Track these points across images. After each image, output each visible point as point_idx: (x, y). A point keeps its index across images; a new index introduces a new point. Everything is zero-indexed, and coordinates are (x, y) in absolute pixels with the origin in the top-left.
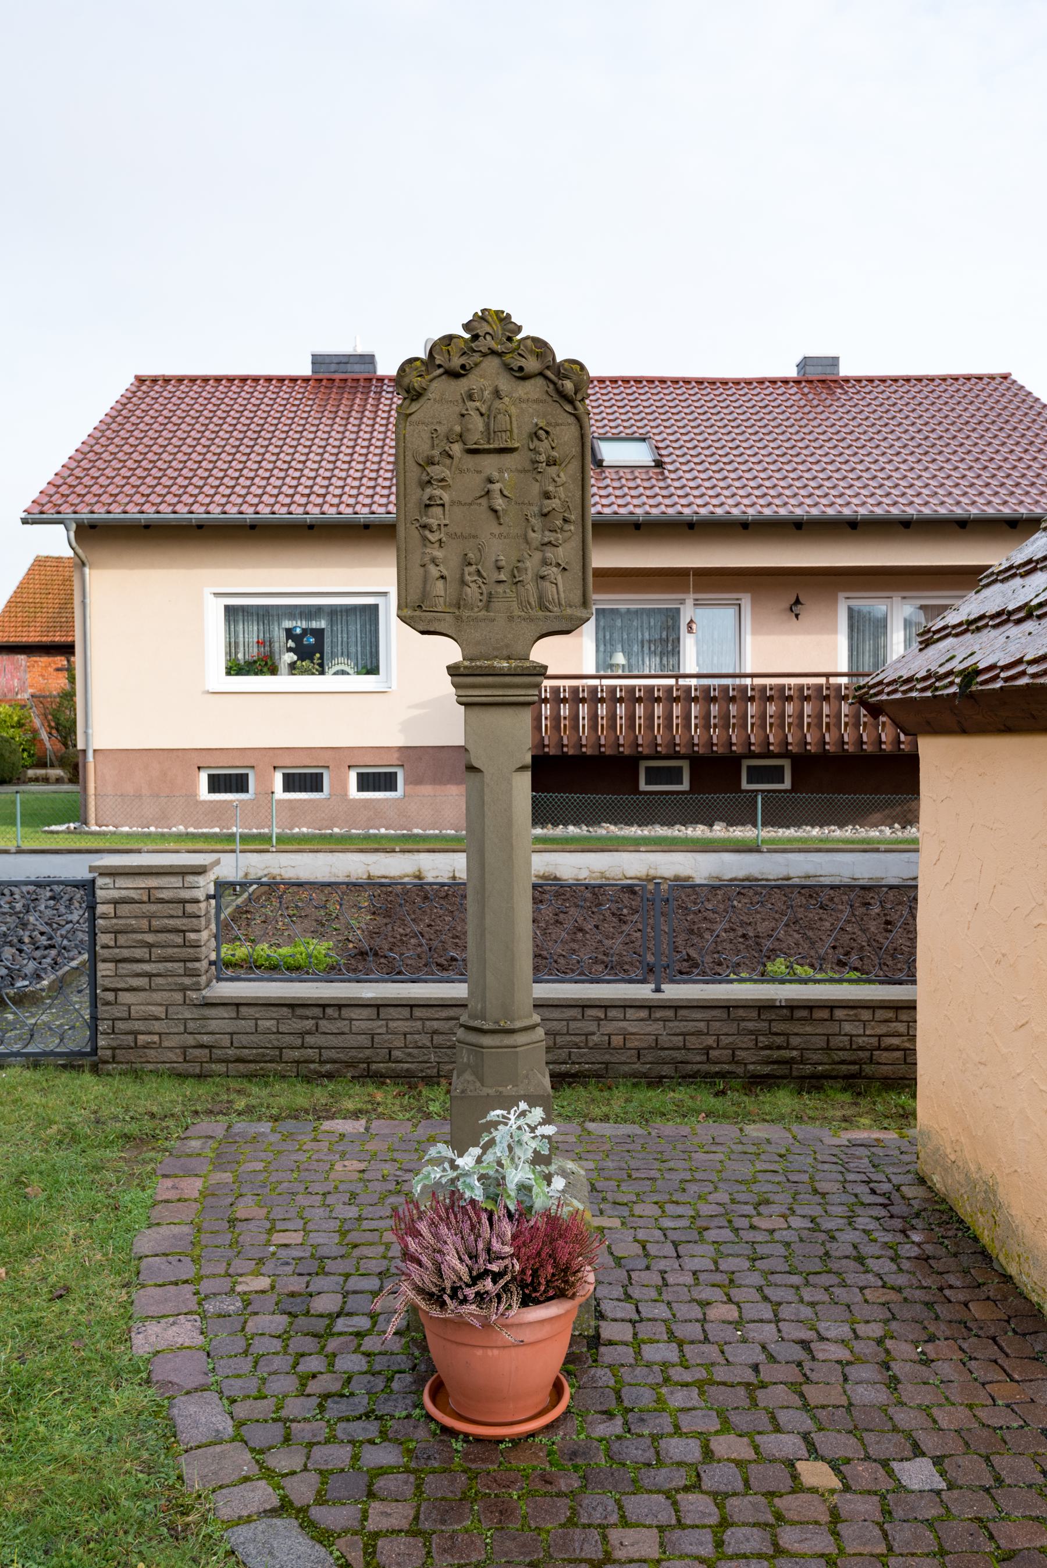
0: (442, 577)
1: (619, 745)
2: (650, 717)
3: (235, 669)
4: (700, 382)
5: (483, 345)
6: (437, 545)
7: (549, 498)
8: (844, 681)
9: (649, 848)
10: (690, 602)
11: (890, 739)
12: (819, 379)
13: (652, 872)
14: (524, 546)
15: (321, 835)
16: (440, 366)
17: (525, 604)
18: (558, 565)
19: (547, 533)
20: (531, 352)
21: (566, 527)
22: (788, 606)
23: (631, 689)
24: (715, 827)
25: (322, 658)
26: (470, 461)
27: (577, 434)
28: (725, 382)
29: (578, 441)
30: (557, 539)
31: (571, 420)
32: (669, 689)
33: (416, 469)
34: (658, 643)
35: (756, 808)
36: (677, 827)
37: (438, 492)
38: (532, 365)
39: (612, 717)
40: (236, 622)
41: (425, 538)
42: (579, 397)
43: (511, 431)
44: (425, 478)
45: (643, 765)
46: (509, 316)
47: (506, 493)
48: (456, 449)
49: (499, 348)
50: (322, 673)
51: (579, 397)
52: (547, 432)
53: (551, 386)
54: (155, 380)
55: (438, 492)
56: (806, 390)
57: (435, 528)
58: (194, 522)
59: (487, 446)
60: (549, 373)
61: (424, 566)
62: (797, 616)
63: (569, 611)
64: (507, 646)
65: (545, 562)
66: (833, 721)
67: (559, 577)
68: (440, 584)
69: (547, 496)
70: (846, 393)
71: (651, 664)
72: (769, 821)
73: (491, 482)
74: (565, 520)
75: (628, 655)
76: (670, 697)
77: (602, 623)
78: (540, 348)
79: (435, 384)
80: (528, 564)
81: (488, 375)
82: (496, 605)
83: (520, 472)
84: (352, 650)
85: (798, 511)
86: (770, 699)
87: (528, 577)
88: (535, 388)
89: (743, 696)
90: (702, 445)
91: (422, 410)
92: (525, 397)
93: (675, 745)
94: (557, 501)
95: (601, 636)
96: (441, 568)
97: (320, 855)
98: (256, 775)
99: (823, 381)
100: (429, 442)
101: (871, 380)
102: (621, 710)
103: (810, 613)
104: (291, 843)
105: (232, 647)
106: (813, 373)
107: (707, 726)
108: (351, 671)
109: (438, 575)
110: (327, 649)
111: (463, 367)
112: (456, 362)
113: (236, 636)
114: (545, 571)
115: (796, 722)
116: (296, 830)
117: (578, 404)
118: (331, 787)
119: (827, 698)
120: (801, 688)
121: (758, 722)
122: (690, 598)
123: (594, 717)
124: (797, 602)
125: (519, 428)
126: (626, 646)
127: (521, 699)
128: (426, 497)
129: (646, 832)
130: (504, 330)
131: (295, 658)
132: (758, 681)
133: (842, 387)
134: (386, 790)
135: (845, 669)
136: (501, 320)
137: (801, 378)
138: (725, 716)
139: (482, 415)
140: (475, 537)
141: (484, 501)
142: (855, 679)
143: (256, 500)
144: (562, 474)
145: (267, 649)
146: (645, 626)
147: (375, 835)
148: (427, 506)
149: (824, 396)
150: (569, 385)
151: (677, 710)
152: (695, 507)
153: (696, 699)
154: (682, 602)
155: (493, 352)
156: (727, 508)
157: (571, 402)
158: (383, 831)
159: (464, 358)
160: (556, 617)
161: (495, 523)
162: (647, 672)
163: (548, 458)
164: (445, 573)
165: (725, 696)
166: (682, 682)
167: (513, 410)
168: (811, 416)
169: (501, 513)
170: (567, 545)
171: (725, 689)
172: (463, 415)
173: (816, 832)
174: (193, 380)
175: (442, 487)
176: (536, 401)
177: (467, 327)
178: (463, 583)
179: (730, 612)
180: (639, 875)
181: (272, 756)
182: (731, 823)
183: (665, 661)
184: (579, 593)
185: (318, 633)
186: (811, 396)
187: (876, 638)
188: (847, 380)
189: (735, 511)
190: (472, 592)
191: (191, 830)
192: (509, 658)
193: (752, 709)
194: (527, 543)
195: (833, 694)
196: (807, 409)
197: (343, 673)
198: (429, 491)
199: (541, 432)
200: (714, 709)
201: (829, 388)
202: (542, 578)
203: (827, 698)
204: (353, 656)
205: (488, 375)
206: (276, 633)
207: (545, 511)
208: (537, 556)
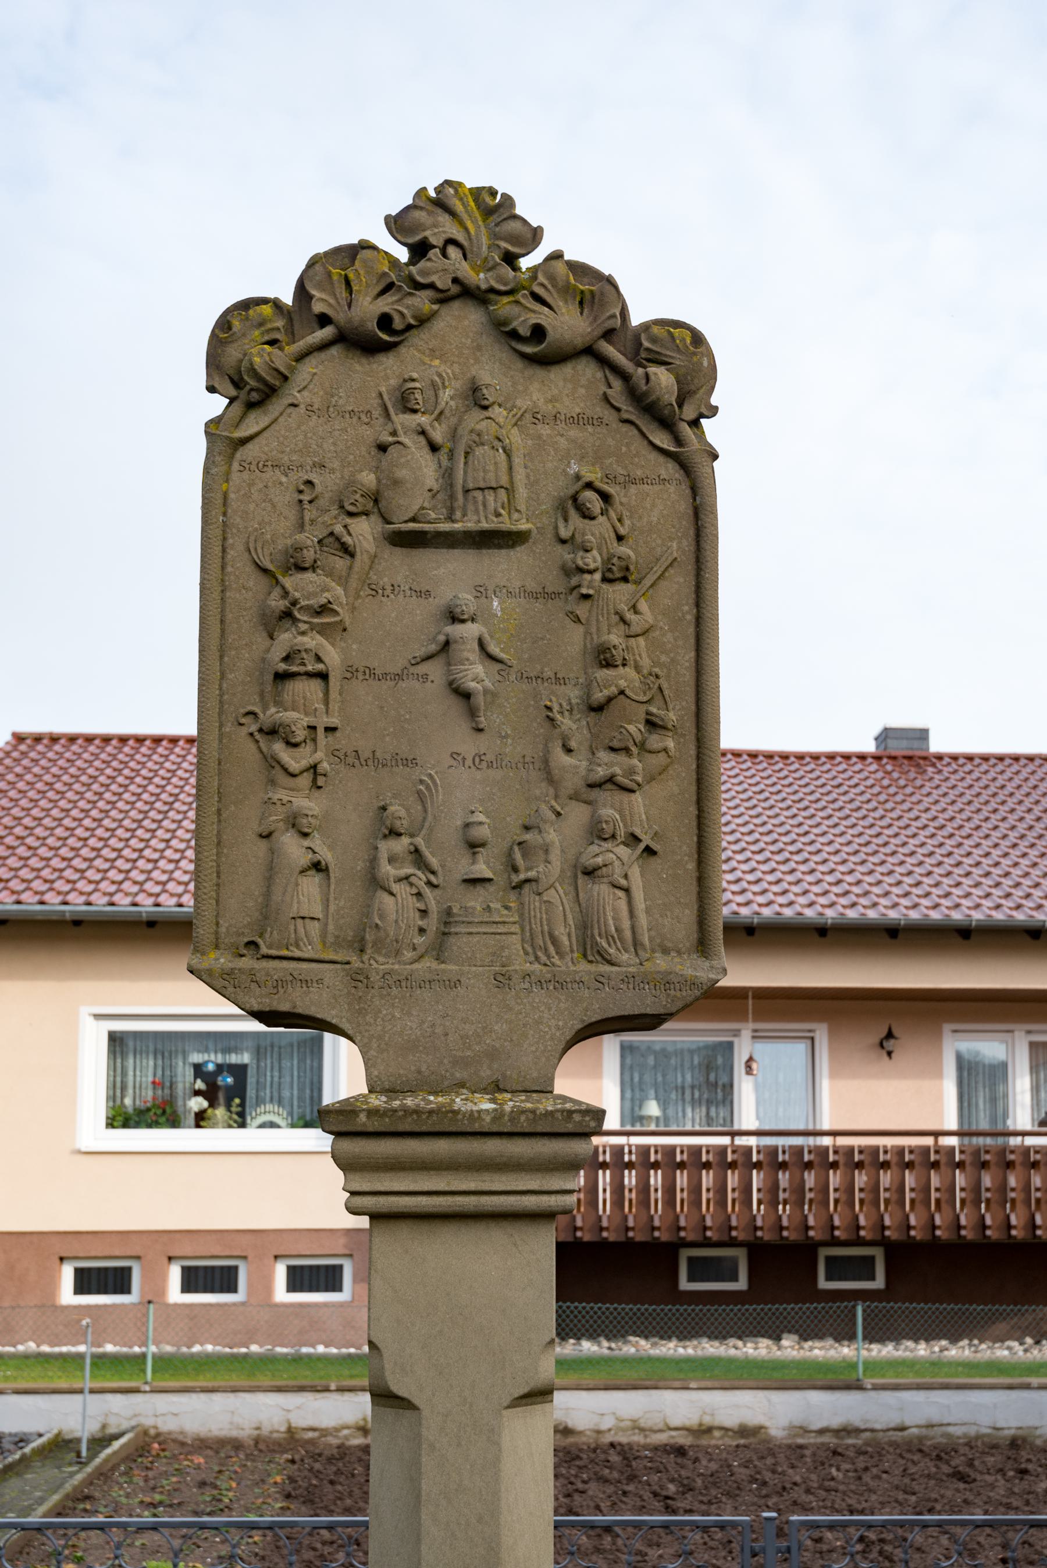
0: (317, 866)
1: (654, 1229)
2: (695, 1189)
3: (121, 1118)
4: (753, 755)
5: (438, 269)
6: (305, 780)
7: (609, 664)
8: (953, 1141)
9: (703, 1384)
10: (746, 1034)
11: (1022, 1223)
12: (904, 755)
13: (707, 1420)
14: (541, 788)
15: (234, 1357)
16: (324, 320)
17: (541, 944)
18: (634, 839)
19: (603, 756)
20: (566, 290)
21: (655, 741)
22: (877, 1040)
23: (671, 1151)
24: (785, 1343)
25: (242, 1105)
26: (400, 566)
27: (684, 506)
28: (785, 757)
29: (686, 524)
30: (631, 772)
31: (669, 469)
32: (722, 1151)
33: (255, 582)
34: (704, 1089)
35: (855, 1324)
36: (732, 1341)
37: (312, 641)
38: (567, 324)
39: (644, 1188)
40: (124, 1057)
41: (273, 763)
42: (689, 413)
43: (510, 490)
44: (277, 603)
45: (685, 1254)
46: (508, 201)
47: (494, 649)
48: (364, 532)
49: (481, 279)
50: (243, 1125)
51: (689, 413)
52: (605, 497)
53: (617, 384)
54: (38, 739)
55: (312, 641)
56: (889, 768)
57: (300, 735)
58: (68, 917)
59: (445, 527)
60: (609, 350)
61: (267, 836)
62: (889, 1054)
63: (661, 963)
64: (493, 1054)
65: (598, 833)
66: (944, 1196)
67: (635, 872)
68: (311, 884)
69: (605, 658)
70: (940, 772)
71: (693, 1118)
72: (871, 1337)
73: (454, 618)
74: (652, 724)
75: (664, 1105)
76: (722, 1162)
77: (628, 1061)
78: (593, 289)
79: (309, 368)
80: (552, 836)
81: (454, 349)
82: (458, 944)
83: (534, 596)
84: (286, 1094)
85: (893, 914)
86: (859, 1165)
87: (552, 870)
88: (574, 387)
89: (823, 1161)
90: (761, 830)
91: (281, 431)
92: (549, 409)
93: (731, 1228)
94: (629, 672)
95: (627, 1078)
96: (316, 842)
97: (217, 1397)
98: (143, 1269)
99: (910, 758)
100: (292, 514)
101: (970, 758)
102: (656, 1179)
103: (906, 1049)
104: (181, 1372)
105: (116, 1089)
106: (897, 747)
107: (774, 1203)
108: (282, 1123)
109: (306, 859)
110: (251, 1092)
111: (385, 321)
112: (367, 308)
113: (124, 1074)
114: (596, 854)
115: (895, 1197)
116: (197, 1348)
117: (686, 430)
118: (250, 1286)
119: (935, 1165)
120: (900, 1151)
121: (844, 1198)
122: (746, 1030)
123: (618, 1189)
124: (890, 1035)
125: (531, 484)
126: (661, 1091)
127: (530, 1202)
128: (278, 652)
129: (690, 1351)
130: (496, 236)
131: (205, 1104)
132: (843, 1141)
133: (934, 765)
134: (327, 1290)
135: (952, 1125)
136: (488, 212)
137: (880, 753)
138: (799, 1189)
139: (434, 448)
140: (410, 762)
141: (435, 670)
142: (966, 1140)
143: (157, 889)
144: (643, 606)
145: (167, 1091)
146: (687, 1064)
147: (309, 1356)
148: (281, 677)
149: (912, 775)
150: (663, 379)
151: (732, 1179)
152: (755, 907)
153: (758, 1165)
154: (737, 1033)
155: (467, 293)
156: (798, 908)
157: (667, 424)
158: (321, 1349)
159: (390, 298)
160: (628, 979)
161: (463, 727)
162: (688, 1127)
163: (608, 561)
164: (326, 855)
165: (796, 1162)
166: (740, 1141)
167: (515, 438)
168: (899, 798)
169: (480, 700)
170: (655, 788)
171: (798, 1151)
172: (383, 448)
173: (922, 1350)
174: (89, 739)
175: (323, 630)
176: (576, 420)
177: (396, 224)
178: (375, 883)
179: (800, 1048)
180: (688, 1423)
181: (165, 1243)
182: (805, 1335)
183: (713, 1110)
184: (689, 915)
185: (239, 1071)
186: (895, 775)
187: (993, 1087)
188: (940, 757)
189: (809, 913)
190: (397, 908)
191: (46, 1348)
192: (496, 1088)
193: (834, 1179)
194: (550, 779)
195: (943, 1160)
196: (892, 790)
197: (272, 1125)
198: (286, 638)
199: (589, 495)
200: (784, 1178)
201: (918, 765)
202: (590, 873)
203: (935, 1165)
204: (286, 1102)
205: (454, 349)
206: (180, 1069)
207: (599, 696)
208: (577, 815)
